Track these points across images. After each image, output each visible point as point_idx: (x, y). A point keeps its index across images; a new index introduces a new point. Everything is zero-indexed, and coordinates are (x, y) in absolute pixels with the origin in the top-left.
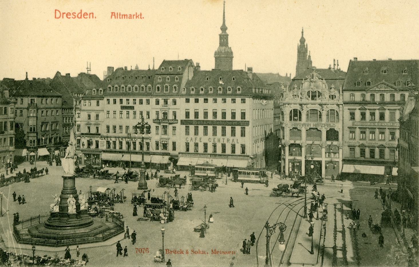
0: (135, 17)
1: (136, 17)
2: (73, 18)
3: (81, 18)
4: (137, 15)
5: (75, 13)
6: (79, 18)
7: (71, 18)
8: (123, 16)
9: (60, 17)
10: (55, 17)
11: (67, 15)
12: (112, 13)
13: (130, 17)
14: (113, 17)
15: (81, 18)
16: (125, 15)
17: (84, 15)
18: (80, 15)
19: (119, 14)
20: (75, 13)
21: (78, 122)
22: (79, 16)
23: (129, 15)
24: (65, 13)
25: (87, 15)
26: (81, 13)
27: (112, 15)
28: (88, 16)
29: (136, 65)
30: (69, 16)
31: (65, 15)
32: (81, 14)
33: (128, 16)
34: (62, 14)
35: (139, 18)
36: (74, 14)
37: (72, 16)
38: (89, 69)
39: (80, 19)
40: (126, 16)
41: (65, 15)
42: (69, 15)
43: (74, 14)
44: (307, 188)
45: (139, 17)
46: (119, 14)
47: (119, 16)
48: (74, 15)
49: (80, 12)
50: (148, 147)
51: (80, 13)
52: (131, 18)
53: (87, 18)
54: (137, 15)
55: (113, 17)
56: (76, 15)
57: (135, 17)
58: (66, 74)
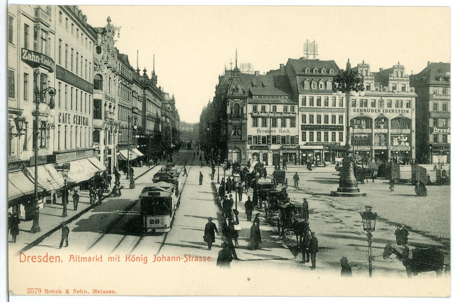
0: (95, 259)
1: (96, 260)
2: (38, 261)
3: (47, 261)
4: (97, 258)
5: (41, 256)
6: (45, 262)
7: (37, 262)
8: (83, 259)
9: (25, 260)
10: (21, 261)
11: (32, 258)
12: (71, 256)
13: (90, 260)
14: (72, 259)
15: (47, 261)
16: (111, 258)
17: (50, 258)
18: (46, 258)
19: (78, 257)
20: (41, 256)
21: (62, 165)
22: (45, 260)
23: (89, 258)
24: (30, 256)
25: (53, 258)
26: (47, 256)
27: (71, 258)
28: (54, 260)
29: (306, 42)
30: (34, 260)
31: (30, 258)
32: (47, 258)
33: (88, 259)
34: (27, 257)
35: (99, 261)
36: (39, 257)
37: (37, 259)
38: (311, 47)
39: (46, 262)
40: (112, 259)
41: (30, 258)
42: (52, 258)
43: (39, 257)
44: (56, 188)
45: (100, 259)
46: (78, 257)
47: (78, 259)
48: (39, 258)
49: (46, 255)
50: (201, 178)
51: (46, 256)
52: (170, 260)
53: (210, 261)
54: (97, 258)
55: (72, 259)
56: (42, 259)
57: (95, 259)
58: (157, 76)
